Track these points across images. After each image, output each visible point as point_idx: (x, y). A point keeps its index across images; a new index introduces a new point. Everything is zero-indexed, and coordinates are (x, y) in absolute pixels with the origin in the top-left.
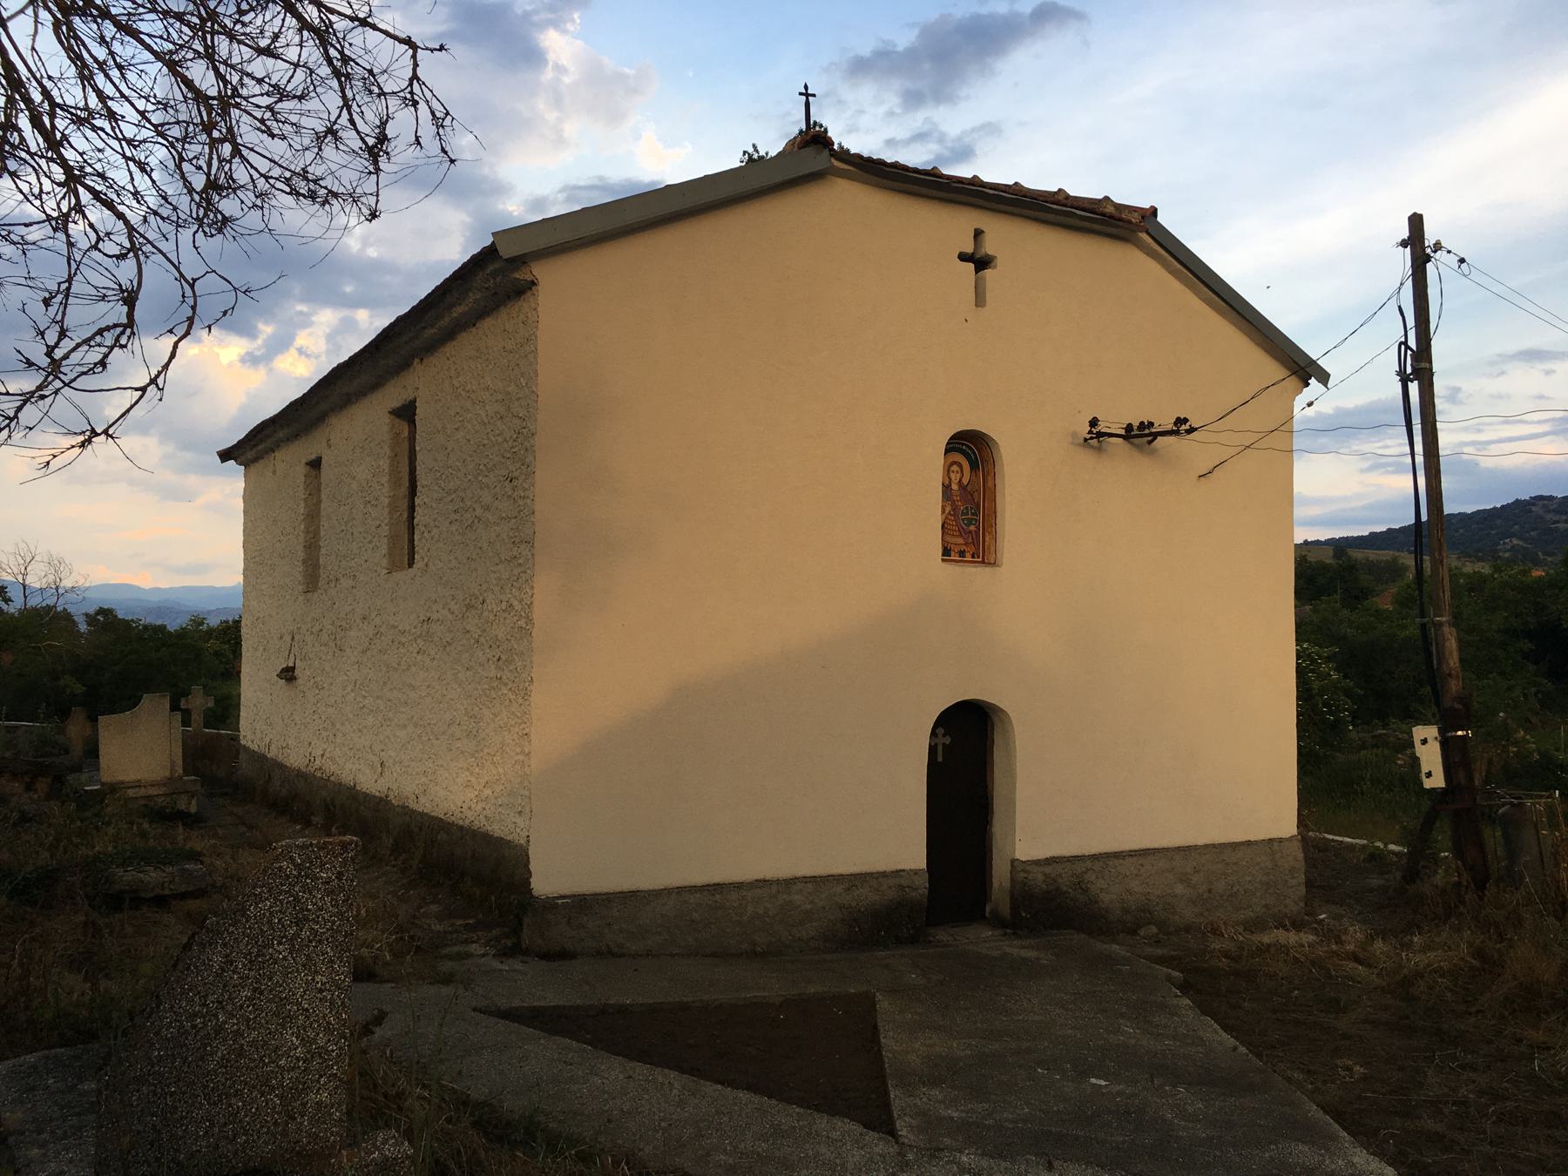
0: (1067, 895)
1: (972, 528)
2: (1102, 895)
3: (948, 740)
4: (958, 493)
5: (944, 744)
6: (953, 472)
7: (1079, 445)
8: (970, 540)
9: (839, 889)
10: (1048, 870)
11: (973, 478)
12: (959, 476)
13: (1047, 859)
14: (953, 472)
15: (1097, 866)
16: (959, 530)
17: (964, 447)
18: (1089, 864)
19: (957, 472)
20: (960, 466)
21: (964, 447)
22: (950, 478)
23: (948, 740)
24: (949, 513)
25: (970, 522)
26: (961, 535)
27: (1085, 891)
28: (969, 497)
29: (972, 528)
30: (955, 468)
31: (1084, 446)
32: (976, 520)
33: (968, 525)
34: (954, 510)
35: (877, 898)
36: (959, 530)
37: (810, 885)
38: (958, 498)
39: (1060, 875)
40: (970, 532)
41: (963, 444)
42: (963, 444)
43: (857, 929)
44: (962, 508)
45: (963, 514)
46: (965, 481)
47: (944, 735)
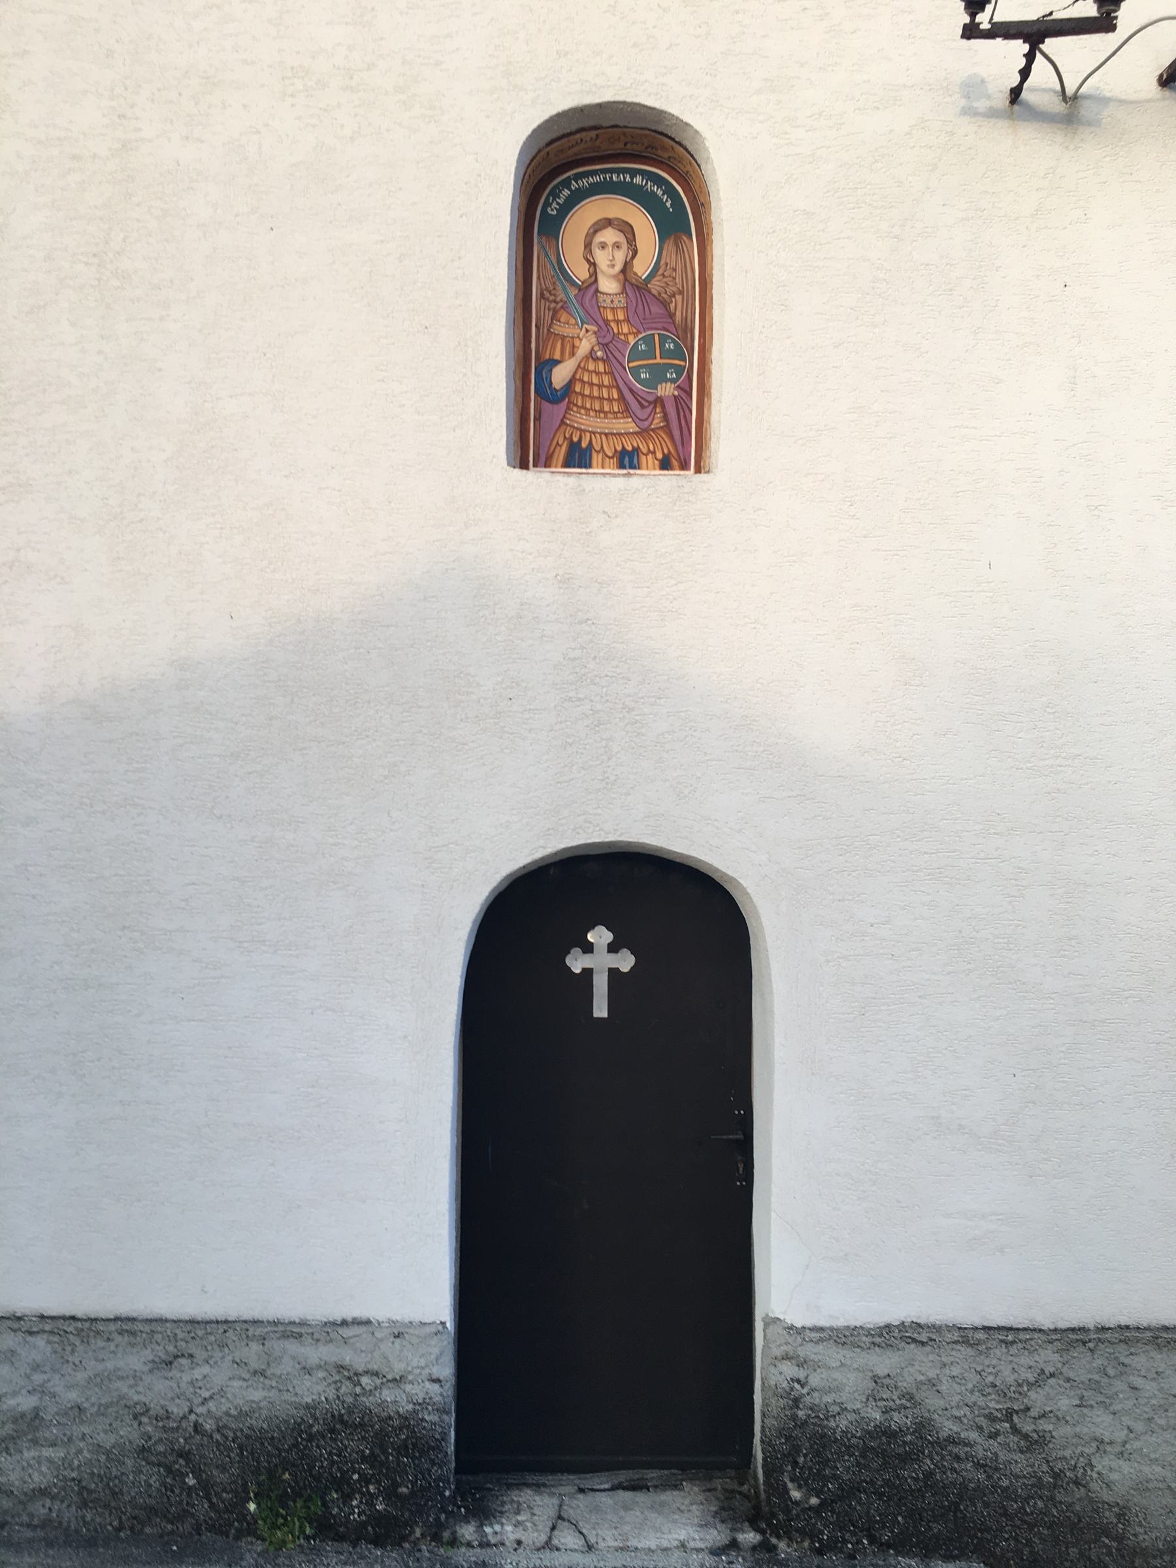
0: (961, 1451)
1: (666, 390)
2: (1101, 1464)
3: (625, 962)
4: (620, 301)
5: (613, 973)
6: (603, 246)
7: (993, 114)
8: (657, 422)
9: (135, 1360)
10: (883, 1363)
11: (670, 257)
12: (620, 256)
13: (888, 1326)
14: (603, 246)
15: (1083, 1366)
16: (622, 397)
17: (638, 180)
18: (1048, 1358)
19: (617, 246)
20: (627, 230)
21: (638, 180)
22: (593, 265)
23: (625, 962)
24: (591, 355)
25: (658, 374)
26: (627, 411)
27: (1034, 1443)
28: (656, 309)
29: (666, 390)
30: (609, 236)
31: (1011, 116)
32: (679, 370)
33: (652, 383)
34: (605, 346)
35: (257, 1395)
36: (622, 397)
37: (40, 1341)
38: (621, 317)
39: (932, 1383)
40: (659, 401)
41: (633, 173)
42: (633, 173)
43: (191, 1481)
44: (632, 340)
45: (635, 354)
46: (642, 268)
47: (613, 948)
